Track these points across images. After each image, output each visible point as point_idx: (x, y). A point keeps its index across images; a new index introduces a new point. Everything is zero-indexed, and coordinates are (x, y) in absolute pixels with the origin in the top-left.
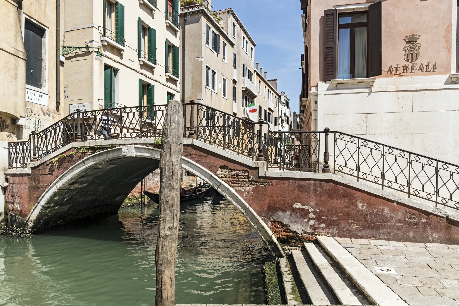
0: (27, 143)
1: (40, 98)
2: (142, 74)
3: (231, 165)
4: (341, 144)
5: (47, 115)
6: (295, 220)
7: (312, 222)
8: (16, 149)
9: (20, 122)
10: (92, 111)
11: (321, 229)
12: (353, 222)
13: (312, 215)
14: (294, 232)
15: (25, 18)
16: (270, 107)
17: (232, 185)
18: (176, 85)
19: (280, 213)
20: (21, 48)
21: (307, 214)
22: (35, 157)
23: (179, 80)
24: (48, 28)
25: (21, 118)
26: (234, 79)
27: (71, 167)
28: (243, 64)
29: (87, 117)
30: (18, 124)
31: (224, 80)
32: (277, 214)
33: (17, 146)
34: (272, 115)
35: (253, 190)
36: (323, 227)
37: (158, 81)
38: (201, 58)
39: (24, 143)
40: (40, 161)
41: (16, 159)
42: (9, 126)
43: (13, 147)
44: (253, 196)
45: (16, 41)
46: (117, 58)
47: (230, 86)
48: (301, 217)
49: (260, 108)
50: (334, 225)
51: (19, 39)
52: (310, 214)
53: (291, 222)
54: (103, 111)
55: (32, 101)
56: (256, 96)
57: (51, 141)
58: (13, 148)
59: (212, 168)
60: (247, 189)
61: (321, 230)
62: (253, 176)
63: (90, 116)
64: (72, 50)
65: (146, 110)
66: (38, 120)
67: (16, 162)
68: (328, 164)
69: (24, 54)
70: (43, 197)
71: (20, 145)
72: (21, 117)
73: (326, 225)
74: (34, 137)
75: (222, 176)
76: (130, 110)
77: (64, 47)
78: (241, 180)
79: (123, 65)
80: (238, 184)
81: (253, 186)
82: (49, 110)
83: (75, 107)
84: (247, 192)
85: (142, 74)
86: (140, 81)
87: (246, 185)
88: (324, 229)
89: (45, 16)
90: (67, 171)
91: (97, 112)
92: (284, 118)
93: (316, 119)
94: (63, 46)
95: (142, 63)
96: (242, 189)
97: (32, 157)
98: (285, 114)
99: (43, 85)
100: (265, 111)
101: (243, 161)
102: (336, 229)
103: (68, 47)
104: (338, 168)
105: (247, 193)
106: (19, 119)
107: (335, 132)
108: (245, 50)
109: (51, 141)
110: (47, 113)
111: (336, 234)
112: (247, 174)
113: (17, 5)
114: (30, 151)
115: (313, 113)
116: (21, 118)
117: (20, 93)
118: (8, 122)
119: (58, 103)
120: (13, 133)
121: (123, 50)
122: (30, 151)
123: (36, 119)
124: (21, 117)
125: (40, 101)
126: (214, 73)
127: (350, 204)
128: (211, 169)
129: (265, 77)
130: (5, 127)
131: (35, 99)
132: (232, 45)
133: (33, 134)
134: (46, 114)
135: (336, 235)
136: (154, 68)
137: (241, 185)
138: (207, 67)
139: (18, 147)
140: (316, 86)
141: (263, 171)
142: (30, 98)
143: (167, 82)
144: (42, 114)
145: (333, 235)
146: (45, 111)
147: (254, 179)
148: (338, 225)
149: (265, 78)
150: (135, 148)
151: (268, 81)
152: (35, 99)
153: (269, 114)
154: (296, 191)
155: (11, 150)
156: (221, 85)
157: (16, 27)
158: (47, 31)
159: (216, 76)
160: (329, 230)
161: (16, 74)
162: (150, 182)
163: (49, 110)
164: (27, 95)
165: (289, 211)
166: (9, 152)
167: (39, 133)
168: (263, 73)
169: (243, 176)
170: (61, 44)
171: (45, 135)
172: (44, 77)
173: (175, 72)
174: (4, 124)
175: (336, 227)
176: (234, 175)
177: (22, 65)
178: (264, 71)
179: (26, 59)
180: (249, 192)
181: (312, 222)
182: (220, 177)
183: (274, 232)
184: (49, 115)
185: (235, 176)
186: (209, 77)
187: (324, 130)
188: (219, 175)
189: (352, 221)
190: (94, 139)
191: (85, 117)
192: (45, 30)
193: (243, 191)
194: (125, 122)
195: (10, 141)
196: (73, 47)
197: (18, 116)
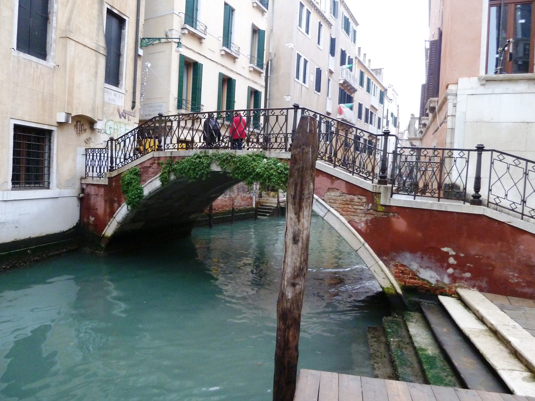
0: (104, 150)
4: (500, 168)
5: (123, 118)
6: (427, 265)
7: (450, 271)
8: (93, 156)
13: (452, 261)
14: (423, 280)
15: (108, 8)
16: (374, 105)
17: (344, 213)
19: (408, 255)
20: (102, 43)
23: (264, 71)
26: (330, 69)
27: (150, 180)
28: (308, 34)
33: (101, 152)
34: (375, 115)
38: (291, 44)
39: (101, 150)
40: (118, 171)
41: (93, 167)
43: (90, 154)
45: (98, 35)
49: (360, 106)
53: (421, 267)
56: (357, 90)
57: (129, 149)
58: (89, 155)
67: (93, 171)
68: (479, 193)
70: (117, 213)
71: (97, 152)
74: (112, 143)
82: (125, 112)
86: (221, 74)
90: (146, 184)
92: (390, 119)
93: (453, 128)
97: (109, 166)
98: (392, 114)
100: (367, 110)
101: (360, 184)
103: (147, 38)
104: (494, 199)
106: (97, 122)
107: (492, 151)
109: (129, 149)
110: (123, 115)
111: (485, 288)
114: (107, 159)
115: (449, 119)
116: (99, 122)
117: (99, 93)
119: (134, 102)
122: (107, 159)
129: (369, 66)
130: (83, 132)
133: (112, 139)
134: (121, 116)
135: (485, 290)
139: (95, 154)
141: (386, 197)
145: (481, 290)
146: (121, 113)
151: (372, 70)
153: (372, 113)
155: (88, 157)
160: (475, 282)
161: (96, 73)
162: (226, 198)
163: (125, 112)
166: (86, 159)
167: (117, 139)
168: (367, 61)
170: (141, 36)
171: (123, 142)
173: (260, 64)
174: (83, 128)
177: (102, 61)
179: (106, 55)
181: (450, 271)
182: (328, 202)
184: (125, 118)
186: (141, 9)
197: (96, 120)
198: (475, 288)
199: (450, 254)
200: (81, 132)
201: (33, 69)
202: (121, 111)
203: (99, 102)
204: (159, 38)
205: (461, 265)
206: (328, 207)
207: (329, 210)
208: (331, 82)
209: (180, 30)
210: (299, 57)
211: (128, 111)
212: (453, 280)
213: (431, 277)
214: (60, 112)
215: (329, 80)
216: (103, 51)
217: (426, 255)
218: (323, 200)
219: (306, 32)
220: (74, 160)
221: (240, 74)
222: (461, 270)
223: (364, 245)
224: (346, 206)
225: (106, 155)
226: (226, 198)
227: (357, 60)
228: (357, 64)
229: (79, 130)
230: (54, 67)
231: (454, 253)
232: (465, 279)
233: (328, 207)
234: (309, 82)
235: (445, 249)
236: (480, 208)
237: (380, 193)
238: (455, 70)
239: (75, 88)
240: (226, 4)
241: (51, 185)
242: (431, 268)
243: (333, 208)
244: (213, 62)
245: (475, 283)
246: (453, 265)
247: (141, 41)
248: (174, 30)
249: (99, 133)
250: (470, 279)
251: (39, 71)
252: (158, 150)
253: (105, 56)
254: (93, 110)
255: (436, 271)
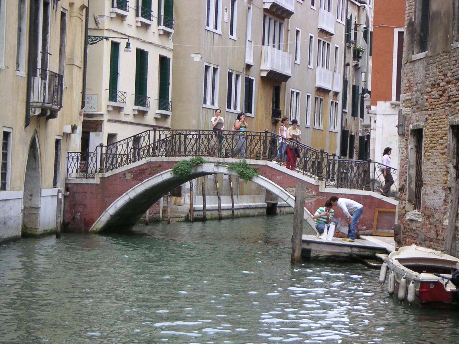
53: (341, 225)
206: (289, 194)
207: (289, 197)
214: (66, 124)
218: (286, 190)
221: (151, 43)
223: (310, 216)
233: (289, 194)
241: (7, 188)
248: (105, 17)
252: (153, 156)
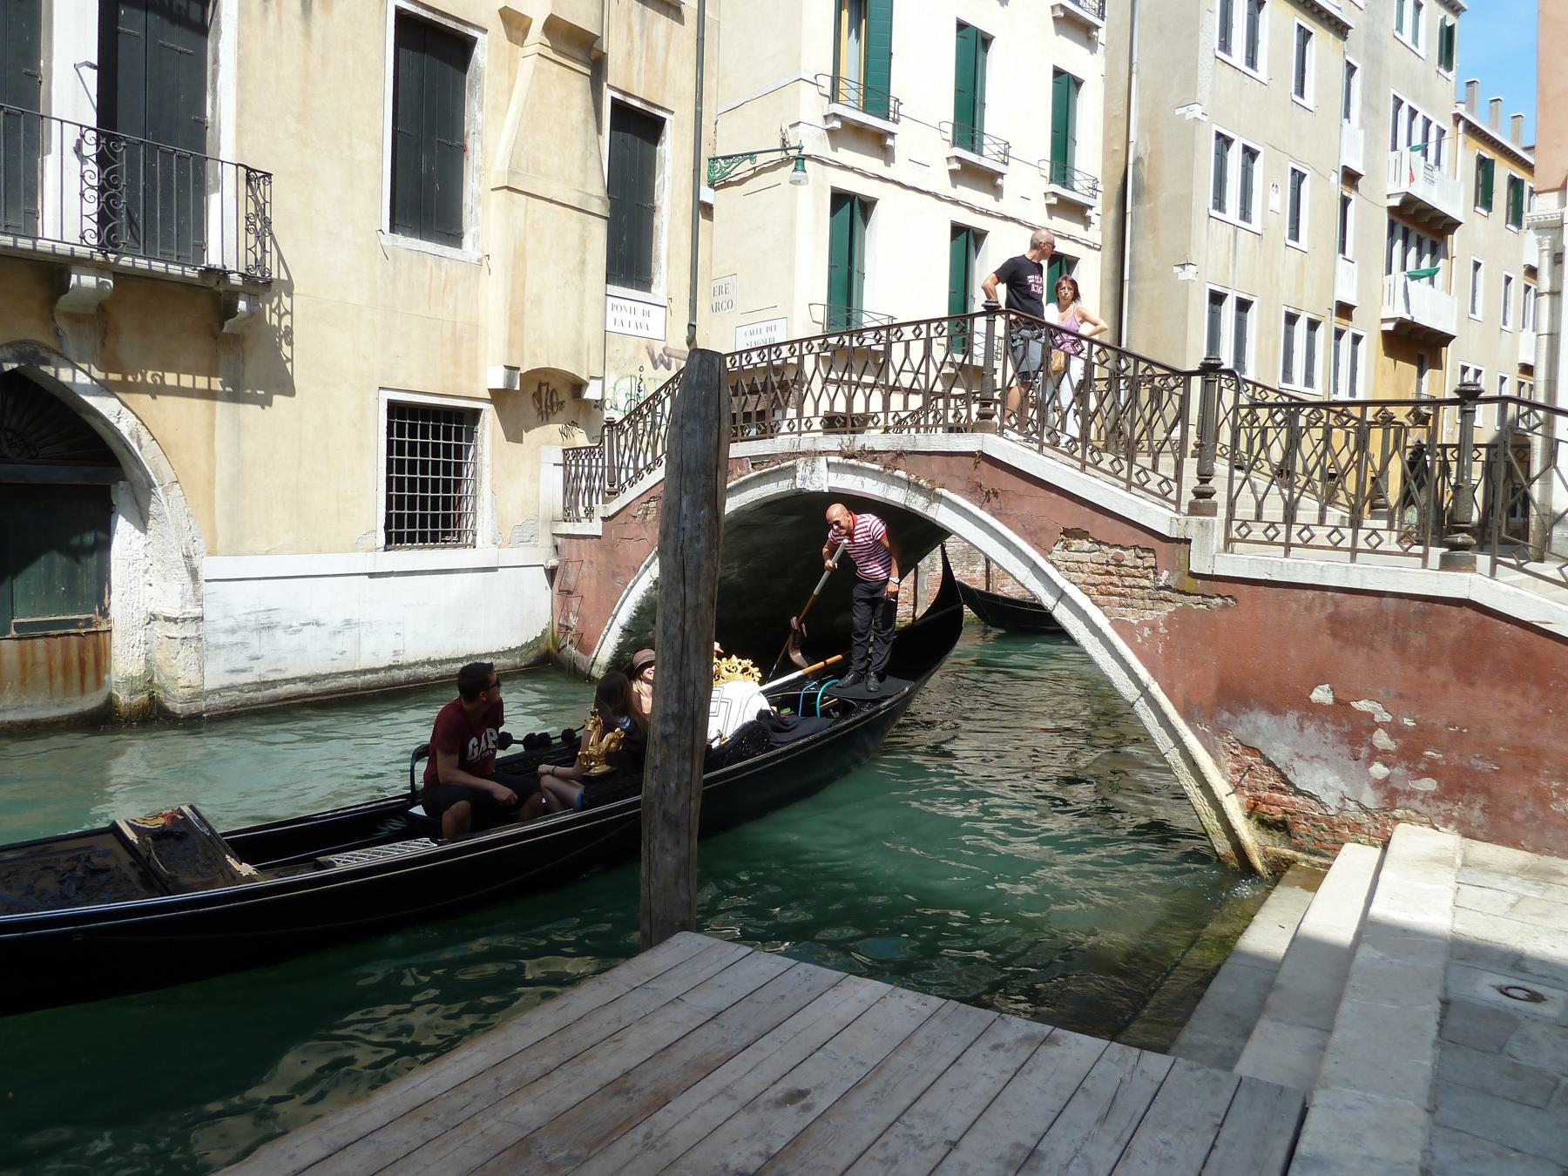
1: (645, 320)
2: (956, 203)
3: (1100, 524)
6: (1314, 752)
9: (591, 393)
10: (792, 343)
11: (1420, 797)
12: (1557, 789)
13: (1382, 739)
18: (1087, 222)
19: (1263, 720)
21: (1364, 732)
22: (612, 489)
24: (672, 112)
25: (592, 382)
26: (1345, 167)
29: (779, 362)
30: (585, 397)
31: (1298, 177)
32: (1250, 722)
35: (1169, 621)
36: (1426, 793)
37: (1013, 220)
38: (1191, 107)
42: (566, 404)
44: (1168, 645)
46: (873, 164)
47: (1320, 195)
48: (1341, 743)
50: (1475, 791)
51: (593, 163)
52: (1375, 734)
53: (1300, 756)
54: (821, 341)
55: (625, 330)
59: (1040, 535)
60: (1148, 616)
61: (1416, 804)
62: (1172, 571)
63: (870, 346)
64: (734, 165)
65: (945, 333)
66: (638, 381)
69: (603, 201)
72: (592, 378)
73: (1439, 784)
75: (1068, 564)
76: (914, 331)
77: (714, 159)
78: (1128, 582)
79: (893, 182)
80: (1120, 595)
81: (1169, 608)
82: (668, 352)
83: (748, 333)
84: (1146, 629)
85: (956, 203)
87: (1147, 601)
88: (1431, 801)
89: (664, 80)
91: (805, 344)
94: (712, 156)
95: (957, 166)
96: (1131, 617)
99: (655, 281)
102: (1481, 809)
103: (724, 158)
105: (1147, 632)
106: (587, 384)
108: (1407, 37)
111: (1479, 827)
112: (1151, 561)
113: (588, 72)
116: (592, 382)
118: (564, 395)
120: (574, 424)
121: (892, 135)
123: (633, 380)
124: (592, 378)
125: (644, 326)
126: (1250, 154)
127: (1545, 712)
128: (1035, 540)
130: (555, 409)
131: (633, 325)
132: (1340, 28)
135: (1480, 835)
136: (1001, 175)
137: (1129, 601)
138: (1219, 135)
140: (1559, 186)
142: (618, 322)
143: (1050, 217)
144: (648, 365)
146: (656, 356)
147: (1171, 583)
148: (1487, 791)
149: (1516, 140)
150: (828, 465)
152: (633, 325)
154: (1326, 640)
156: (1280, 201)
157: (586, 131)
158: (667, 123)
159: (1258, 166)
161: (583, 262)
162: (974, 571)
163: (668, 352)
164: (611, 315)
165: (1296, 714)
168: (1506, 122)
169: (1136, 567)
172: (658, 258)
174: (555, 400)
175: (1481, 800)
176: (1108, 564)
178: (1507, 112)
180: (1153, 628)
183: (1237, 787)
185: (1111, 568)
187: (1457, 392)
188: (1058, 563)
189: (1555, 784)
190: (795, 433)
191: (775, 363)
192: (663, 120)
193: (1136, 622)
194: (810, 384)
195: (569, 444)
196: (736, 156)
197: (584, 377)
198: (1451, 826)
199: (1377, 718)
200: (549, 411)
201: (428, 270)
202: (658, 352)
203: (592, 335)
204: (752, 154)
205: (1410, 752)
208: (1351, 208)
209: (820, 122)
210: (1224, 141)
211: (675, 350)
212: (1385, 798)
213: (1326, 787)
215: (1345, 202)
216: (599, 207)
217: (1311, 719)
219: (1247, 64)
220: (535, 478)
222: (1408, 769)
224: (1107, 579)
225: (600, 463)
226: (974, 571)
227: (1461, 124)
228: (1460, 136)
229: (546, 406)
230: (480, 260)
231: (1389, 718)
232: (1420, 797)
233: (1061, 582)
234: (1264, 216)
235: (1363, 705)
236: (1461, 579)
237: (1188, 541)
238: (1559, 146)
239: (528, 305)
240: (961, 26)
242: (1326, 760)
243: (1075, 584)
244: (924, 196)
245: (1450, 810)
246: (1386, 752)
247: (711, 168)
249: (598, 409)
250: (1437, 797)
251: (443, 274)
253: (606, 218)
254: (577, 354)
255: (1343, 773)
